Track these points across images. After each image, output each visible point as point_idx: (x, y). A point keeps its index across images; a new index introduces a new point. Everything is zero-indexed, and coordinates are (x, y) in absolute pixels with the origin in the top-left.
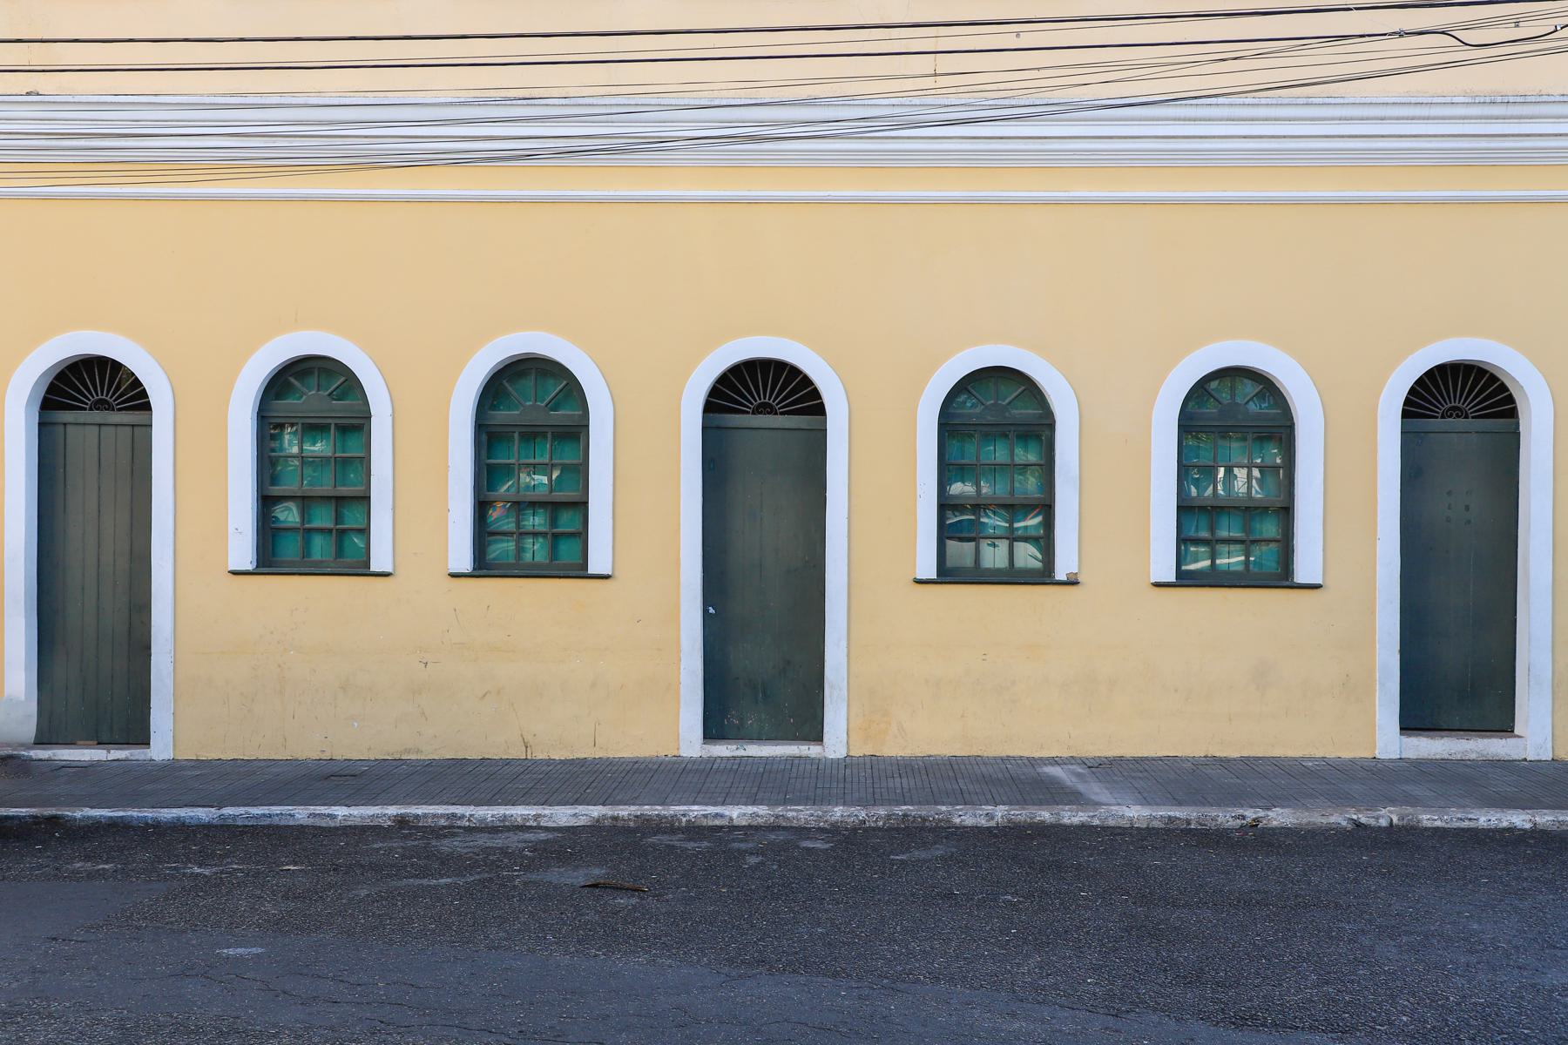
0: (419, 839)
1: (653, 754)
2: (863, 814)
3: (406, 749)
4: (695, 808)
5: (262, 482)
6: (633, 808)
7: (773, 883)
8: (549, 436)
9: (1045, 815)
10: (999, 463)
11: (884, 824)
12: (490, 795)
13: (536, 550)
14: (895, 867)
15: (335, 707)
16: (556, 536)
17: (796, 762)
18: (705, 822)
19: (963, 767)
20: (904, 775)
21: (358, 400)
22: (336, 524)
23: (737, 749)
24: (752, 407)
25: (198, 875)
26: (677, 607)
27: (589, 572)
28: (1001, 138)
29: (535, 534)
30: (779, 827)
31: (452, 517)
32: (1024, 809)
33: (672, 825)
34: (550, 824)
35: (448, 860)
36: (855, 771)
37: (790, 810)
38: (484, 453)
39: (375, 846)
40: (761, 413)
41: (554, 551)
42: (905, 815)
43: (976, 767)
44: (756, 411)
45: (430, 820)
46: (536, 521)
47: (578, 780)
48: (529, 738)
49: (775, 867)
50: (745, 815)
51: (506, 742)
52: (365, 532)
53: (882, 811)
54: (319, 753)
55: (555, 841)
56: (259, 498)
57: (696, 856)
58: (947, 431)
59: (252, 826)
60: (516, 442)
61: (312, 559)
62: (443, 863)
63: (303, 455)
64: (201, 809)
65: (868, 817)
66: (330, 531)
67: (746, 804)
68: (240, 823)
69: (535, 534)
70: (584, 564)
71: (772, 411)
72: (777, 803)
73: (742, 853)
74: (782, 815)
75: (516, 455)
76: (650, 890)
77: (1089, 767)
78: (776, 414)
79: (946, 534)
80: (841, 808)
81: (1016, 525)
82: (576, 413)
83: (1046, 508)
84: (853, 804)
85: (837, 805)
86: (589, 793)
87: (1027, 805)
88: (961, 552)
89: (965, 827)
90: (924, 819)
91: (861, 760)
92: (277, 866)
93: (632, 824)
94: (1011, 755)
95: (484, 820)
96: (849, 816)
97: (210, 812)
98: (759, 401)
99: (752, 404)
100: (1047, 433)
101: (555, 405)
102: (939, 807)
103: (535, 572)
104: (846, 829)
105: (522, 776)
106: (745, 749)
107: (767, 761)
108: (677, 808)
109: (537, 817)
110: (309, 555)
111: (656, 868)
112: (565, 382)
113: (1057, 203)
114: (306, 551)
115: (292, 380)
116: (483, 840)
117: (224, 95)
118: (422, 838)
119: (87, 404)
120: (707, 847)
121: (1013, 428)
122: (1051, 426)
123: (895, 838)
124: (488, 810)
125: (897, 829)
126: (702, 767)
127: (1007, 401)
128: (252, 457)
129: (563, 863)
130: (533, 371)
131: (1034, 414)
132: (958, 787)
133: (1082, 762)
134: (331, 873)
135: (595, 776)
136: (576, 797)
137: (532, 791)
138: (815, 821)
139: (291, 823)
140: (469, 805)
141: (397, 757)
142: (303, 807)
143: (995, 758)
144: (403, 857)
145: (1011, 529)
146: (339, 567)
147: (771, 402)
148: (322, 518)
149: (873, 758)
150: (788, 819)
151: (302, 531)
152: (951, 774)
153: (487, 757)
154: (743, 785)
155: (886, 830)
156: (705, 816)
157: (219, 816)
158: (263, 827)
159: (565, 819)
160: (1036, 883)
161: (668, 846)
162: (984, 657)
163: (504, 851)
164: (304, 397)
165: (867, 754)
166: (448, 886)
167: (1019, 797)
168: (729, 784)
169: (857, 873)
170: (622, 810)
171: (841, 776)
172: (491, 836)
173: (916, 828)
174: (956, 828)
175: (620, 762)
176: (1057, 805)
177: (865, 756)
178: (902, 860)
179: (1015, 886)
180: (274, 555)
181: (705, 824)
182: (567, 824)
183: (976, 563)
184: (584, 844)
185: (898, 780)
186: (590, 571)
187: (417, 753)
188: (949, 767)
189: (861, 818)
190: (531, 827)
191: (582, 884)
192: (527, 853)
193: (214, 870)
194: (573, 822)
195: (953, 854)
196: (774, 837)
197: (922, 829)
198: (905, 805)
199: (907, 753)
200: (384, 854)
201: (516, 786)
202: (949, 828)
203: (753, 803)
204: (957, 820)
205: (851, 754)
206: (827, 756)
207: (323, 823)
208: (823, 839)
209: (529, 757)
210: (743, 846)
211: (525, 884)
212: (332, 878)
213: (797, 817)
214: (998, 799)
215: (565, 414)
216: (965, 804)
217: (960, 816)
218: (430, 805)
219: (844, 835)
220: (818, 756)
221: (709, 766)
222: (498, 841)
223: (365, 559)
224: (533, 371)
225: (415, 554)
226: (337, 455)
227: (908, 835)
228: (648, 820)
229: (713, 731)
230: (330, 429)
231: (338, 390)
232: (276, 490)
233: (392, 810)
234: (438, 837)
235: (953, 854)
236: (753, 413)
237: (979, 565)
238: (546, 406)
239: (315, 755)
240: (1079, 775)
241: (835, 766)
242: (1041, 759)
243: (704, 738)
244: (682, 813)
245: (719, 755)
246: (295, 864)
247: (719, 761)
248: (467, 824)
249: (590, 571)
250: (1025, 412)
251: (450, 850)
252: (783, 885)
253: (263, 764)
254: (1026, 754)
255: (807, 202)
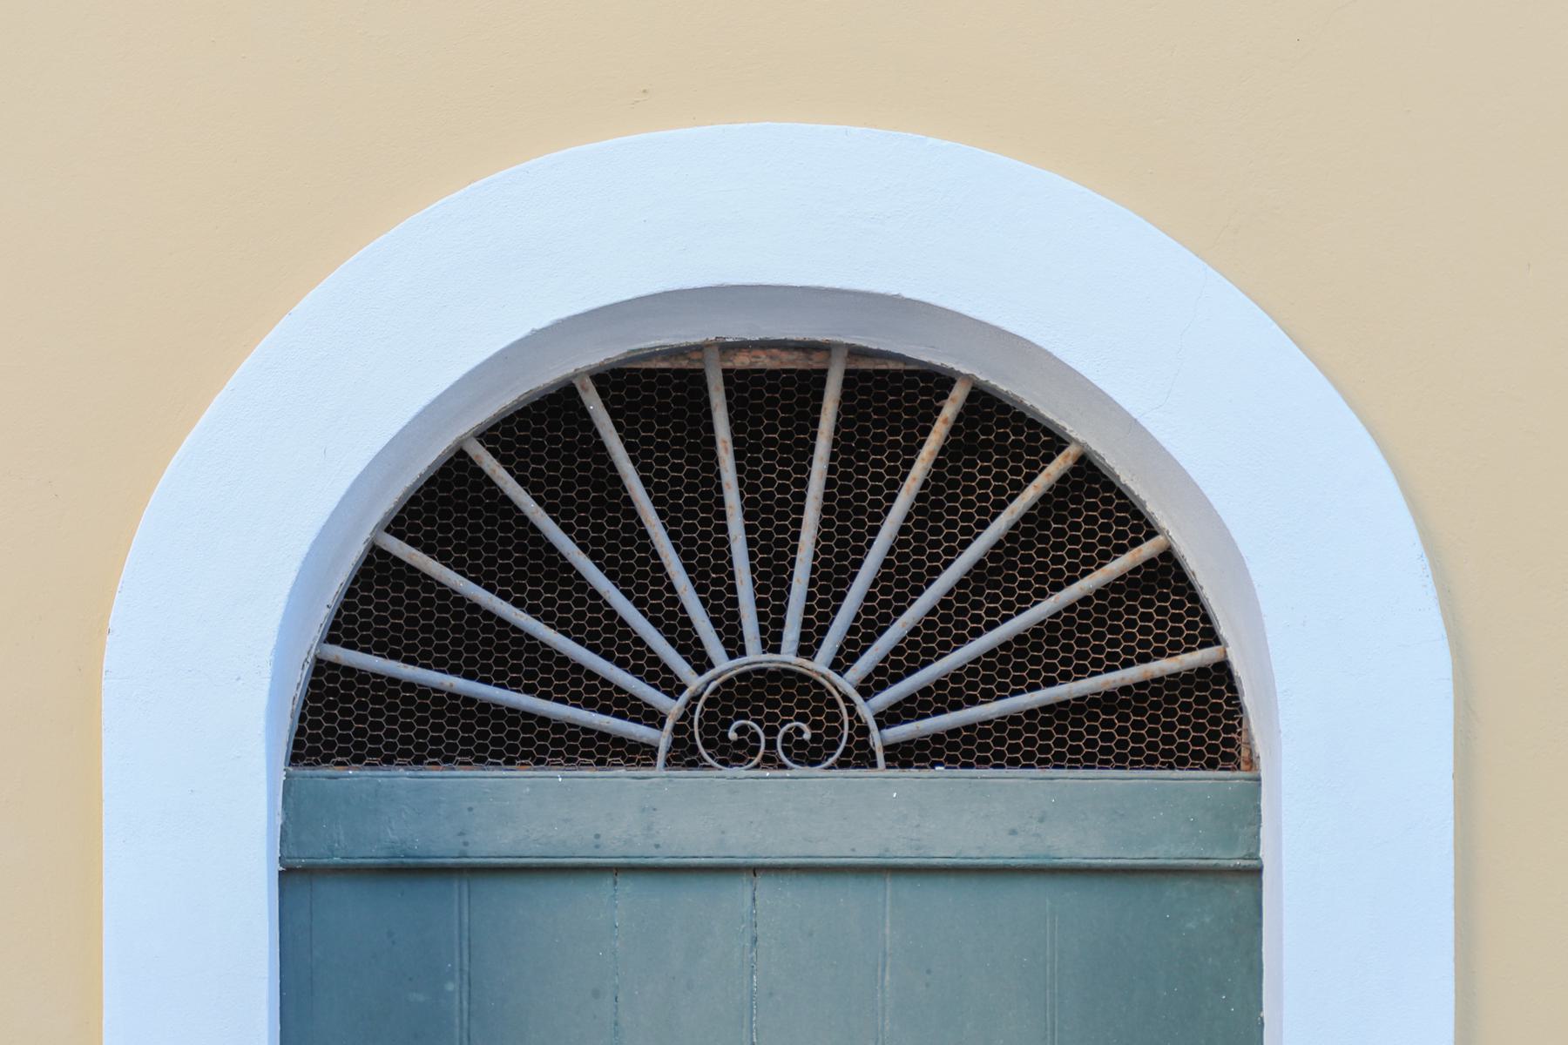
24: (672, 708)
40: (732, 755)
51: (755, 875)
78: (859, 756)
117: (988, 858)
119: (654, 718)
147: (819, 665)
236: (683, 755)
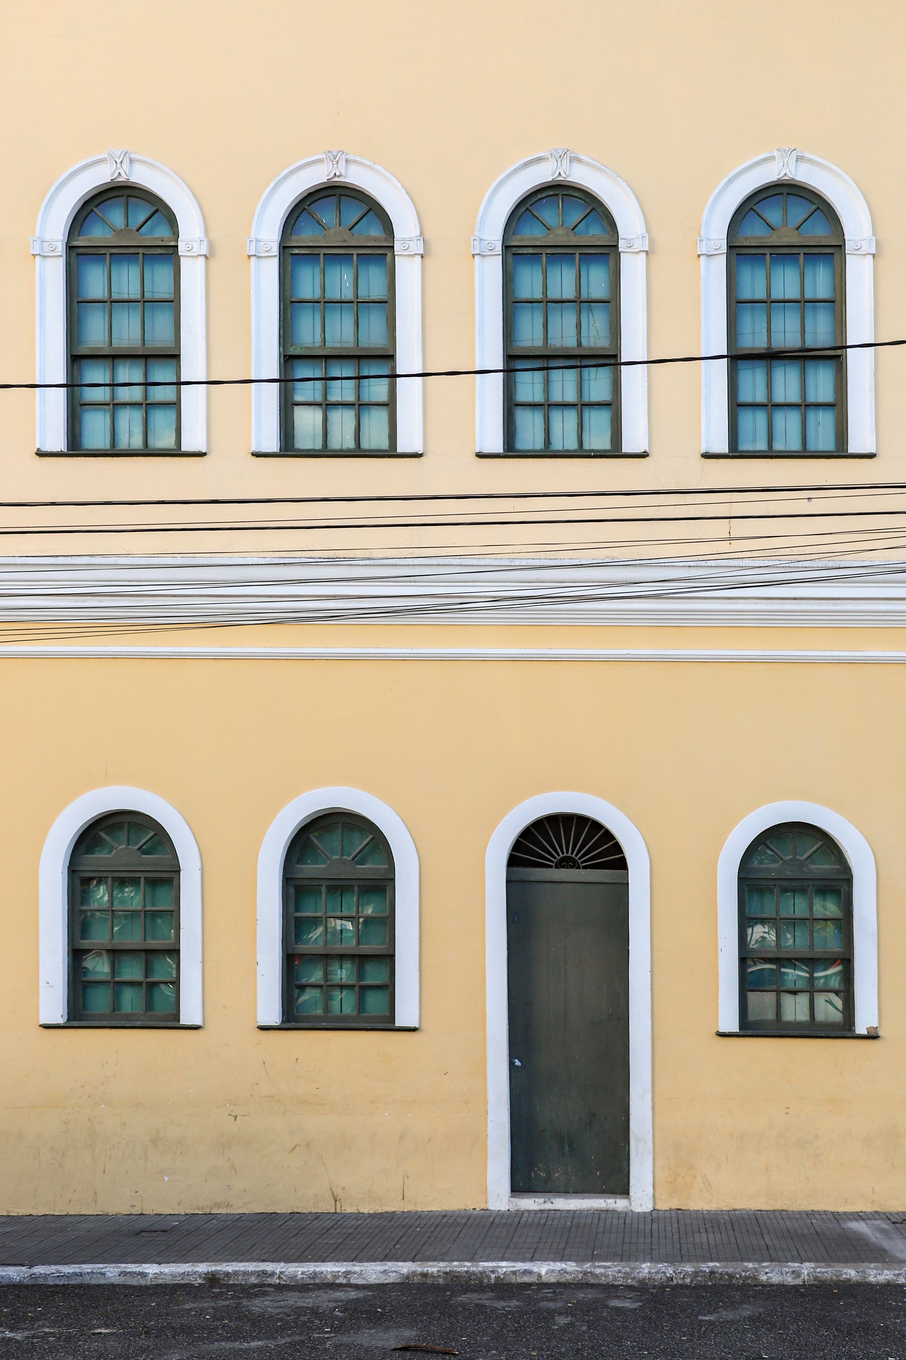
0: (230, 1299)
1: (461, 1207)
2: (670, 1271)
3: (216, 1203)
4: (504, 1264)
5: (73, 934)
6: (442, 1264)
7: (582, 1345)
8: (356, 889)
9: (850, 1273)
10: (799, 916)
11: (692, 1281)
12: (300, 1251)
13: (343, 1002)
14: (703, 1329)
15: (146, 1161)
16: (364, 989)
17: (603, 1215)
18: (514, 1279)
19: (768, 1221)
20: (710, 1230)
21: (168, 854)
22: (146, 977)
23: (545, 1202)
24: (555, 861)
25: (10, 1339)
26: (483, 1059)
27: (397, 1025)
28: (795, 599)
29: (342, 987)
30: (587, 1284)
31: (260, 969)
32: (829, 1266)
33: (482, 1282)
34: (360, 1282)
35: (259, 1321)
36: (662, 1225)
37: (598, 1267)
38: (292, 907)
39: (187, 1306)
40: (563, 867)
41: (361, 1006)
42: (712, 1273)
43: (781, 1222)
44: (561, 864)
45: (240, 1278)
46: (343, 973)
47: (387, 1235)
48: (338, 1192)
49: (584, 1328)
50: (553, 1271)
51: (315, 1196)
52: (176, 983)
53: (689, 1268)
54: (129, 1208)
55: (365, 1300)
56: (71, 951)
57: (506, 1316)
58: (747, 885)
59: (63, 1285)
60: (324, 895)
61: (122, 1012)
62: (253, 1324)
63: (113, 908)
64: (12, 1268)
65: (676, 1274)
66: (140, 984)
67: (554, 1260)
68: (50, 1282)
69: (342, 987)
70: (392, 1018)
71: (576, 865)
72: (584, 1260)
73: (552, 1313)
74: (591, 1272)
75: (324, 908)
76: (461, 1353)
77: (894, 1223)
78: (579, 868)
79: (747, 987)
80: (649, 1264)
81: (816, 975)
82: (383, 866)
83: (846, 962)
84: (659, 1260)
85: (644, 1261)
86: (398, 1249)
87: (833, 1262)
88: (764, 1003)
89: (772, 1285)
90: (731, 1276)
91: (668, 1214)
92: (90, 1329)
93: (441, 1281)
94: (816, 1209)
95: (293, 1277)
96: (656, 1273)
97: (21, 1271)
98: (561, 856)
99: (555, 858)
100: (845, 887)
101: (360, 858)
102: (746, 1264)
103: (343, 1025)
104: (654, 1287)
105: (331, 1231)
106: (552, 1203)
107: (574, 1215)
108: (486, 1264)
109: (348, 1273)
110: (119, 1009)
111: (466, 1329)
112: (371, 837)
113: (851, 662)
114: (116, 1005)
115: (103, 835)
116: (293, 1300)
118: (233, 1297)
120: (517, 1306)
121: (811, 883)
122: (849, 881)
123: (703, 1297)
124: (297, 1267)
125: (705, 1288)
126: (510, 1221)
127: (805, 856)
128: (63, 985)
129: (374, 1324)
130: (340, 825)
131: (833, 869)
132: (764, 1243)
133: (886, 1217)
134: (143, 1336)
135: (404, 1230)
136: (385, 1253)
137: (342, 1247)
138: (623, 1278)
139: (102, 1282)
140: (279, 1261)
141: (207, 1211)
142: (114, 1265)
143: (800, 1213)
144: (214, 1318)
145: (811, 979)
146: (149, 1021)
148: (132, 971)
149: (679, 1212)
150: (596, 1275)
151: (112, 984)
152: (757, 1229)
153: (296, 1210)
154: (550, 1240)
155: (693, 1287)
156: (514, 1273)
157: (31, 1275)
158: (74, 1286)
159: (374, 1276)
160: (844, 1347)
161: (477, 1305)
162: (787, 1111)
163: (314, 1312)
164: (115, 851)
165: (673, 1207)
166: (259, 1349)
167: (825, 1254)
168: (536, 1239)
169: (666, 1335)
170: (431, 1266)
171: (648, 1230)
172: (302, 1294)
173: (723, 1286)
174: (763, 1286)
175: (430, 1215)
176: (863, 1262)
177: (671, 1210)
178: (709, 1321)
179: (823, 1350)
180: (85, 1007)
181: (513, 1281)
182: (377, 1282)
183: (777, 1016)
184: (394, 1303)
185: (704, 1235)
186: (398, 1023)
187: (227, 1207)
188: (754, 1222)
189: (668, 1275)
190: (341, 1285)
191: (393, 1347)
192: (338, 1313)
193: (26, 1334)
194: (383, 1279)
195: (760, 1315)
196: (582, 1295)
197: (730, 1286)
198: (712, 1261)
199: (713, 1206)
200: (195, 1315)
201: (326, 1241)
202: (755, 1286)
203: (562, 1259)
204: (763, 1278)
205: (658, 1207)
206: (633, 1209)
207: (134, 1282)
208: (631, 1298)
209: (338, 1211)
210: (552, 1305)
211: (337, 1347)
212: (142, 1342)
213: (605, 1273)
214: (803, 1254)
215: (371, 868)
216: (772, 1261)
217: (767, 1273)
218: (241, 1261)
219: (652, 1293)
220: (625, 1210)
221: (517, 1220)
222: (308, 1301)
223: (174, 1011)
224: (340, 825)
225: (224, 1007)
226: (147, 908)
227: (717, 1293)
228: (456, 1277)
229: (519, 1187)
230: (140, 883)
231: (149, 844)
232: (85, 944)
233: (203, 1268)
234: (250, 1296)
235: (760, 1315)
236: (556, 867)
237: (780, 1019)
238: (353, 859)
239: (125, 1210)
240: (883, 1231)
241: (642, 1220)
242: (845, 1213)
243: (512, 1191)
244: (491, 1269)
245: (527, 1208)
246: (107, 1327)
247: (526, 1214)
248: (278, 1281)
249: (398, 1023)
250: (824, 867)
251: (261, 1310)
252: (592, 1348)
253: (73, 1220)
254: (831, 1208)
255: (606, 660)
